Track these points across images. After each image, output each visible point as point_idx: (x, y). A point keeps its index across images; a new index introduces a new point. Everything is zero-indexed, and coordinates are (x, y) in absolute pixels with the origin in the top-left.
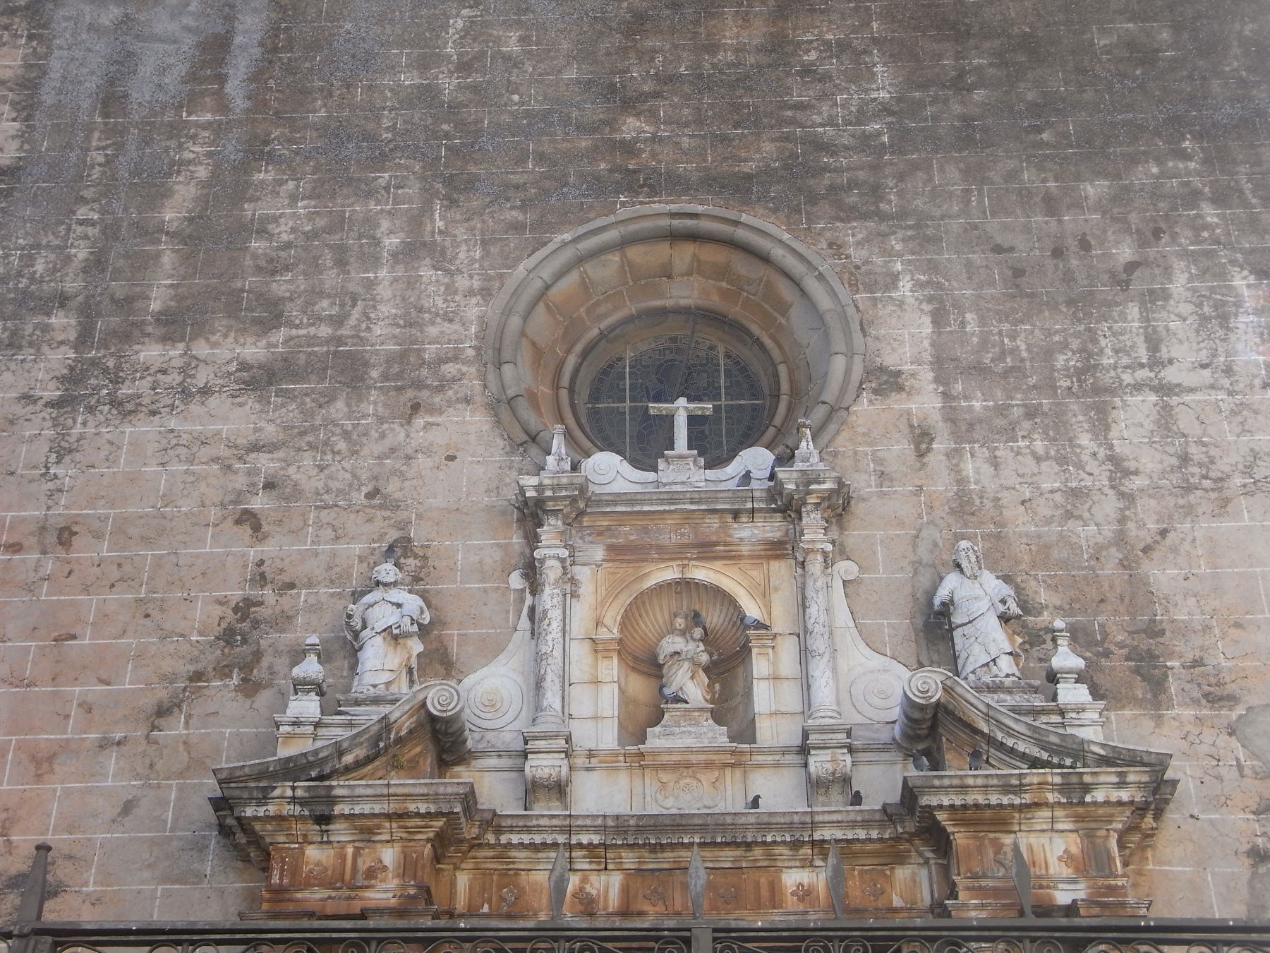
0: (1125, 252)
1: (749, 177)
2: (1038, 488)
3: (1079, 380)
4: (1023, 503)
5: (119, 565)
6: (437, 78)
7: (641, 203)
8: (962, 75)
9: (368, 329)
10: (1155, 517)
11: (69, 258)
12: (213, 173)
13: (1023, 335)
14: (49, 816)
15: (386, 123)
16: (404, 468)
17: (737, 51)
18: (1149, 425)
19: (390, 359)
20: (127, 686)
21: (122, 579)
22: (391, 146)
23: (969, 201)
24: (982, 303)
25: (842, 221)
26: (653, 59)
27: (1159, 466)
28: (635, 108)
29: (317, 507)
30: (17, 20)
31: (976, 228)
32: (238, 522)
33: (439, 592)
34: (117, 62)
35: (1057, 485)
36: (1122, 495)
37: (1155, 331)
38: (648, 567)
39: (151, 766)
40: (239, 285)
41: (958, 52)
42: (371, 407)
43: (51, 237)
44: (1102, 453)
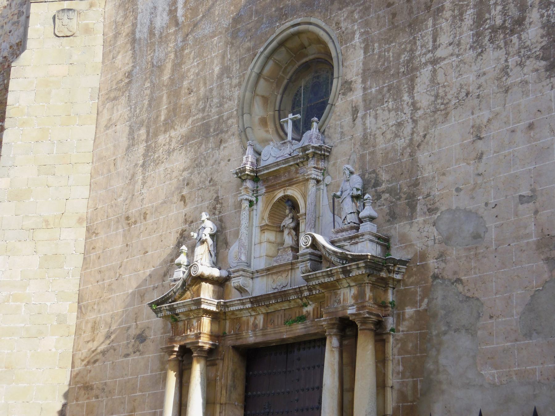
38: (276, 192)
44: (410, 101)
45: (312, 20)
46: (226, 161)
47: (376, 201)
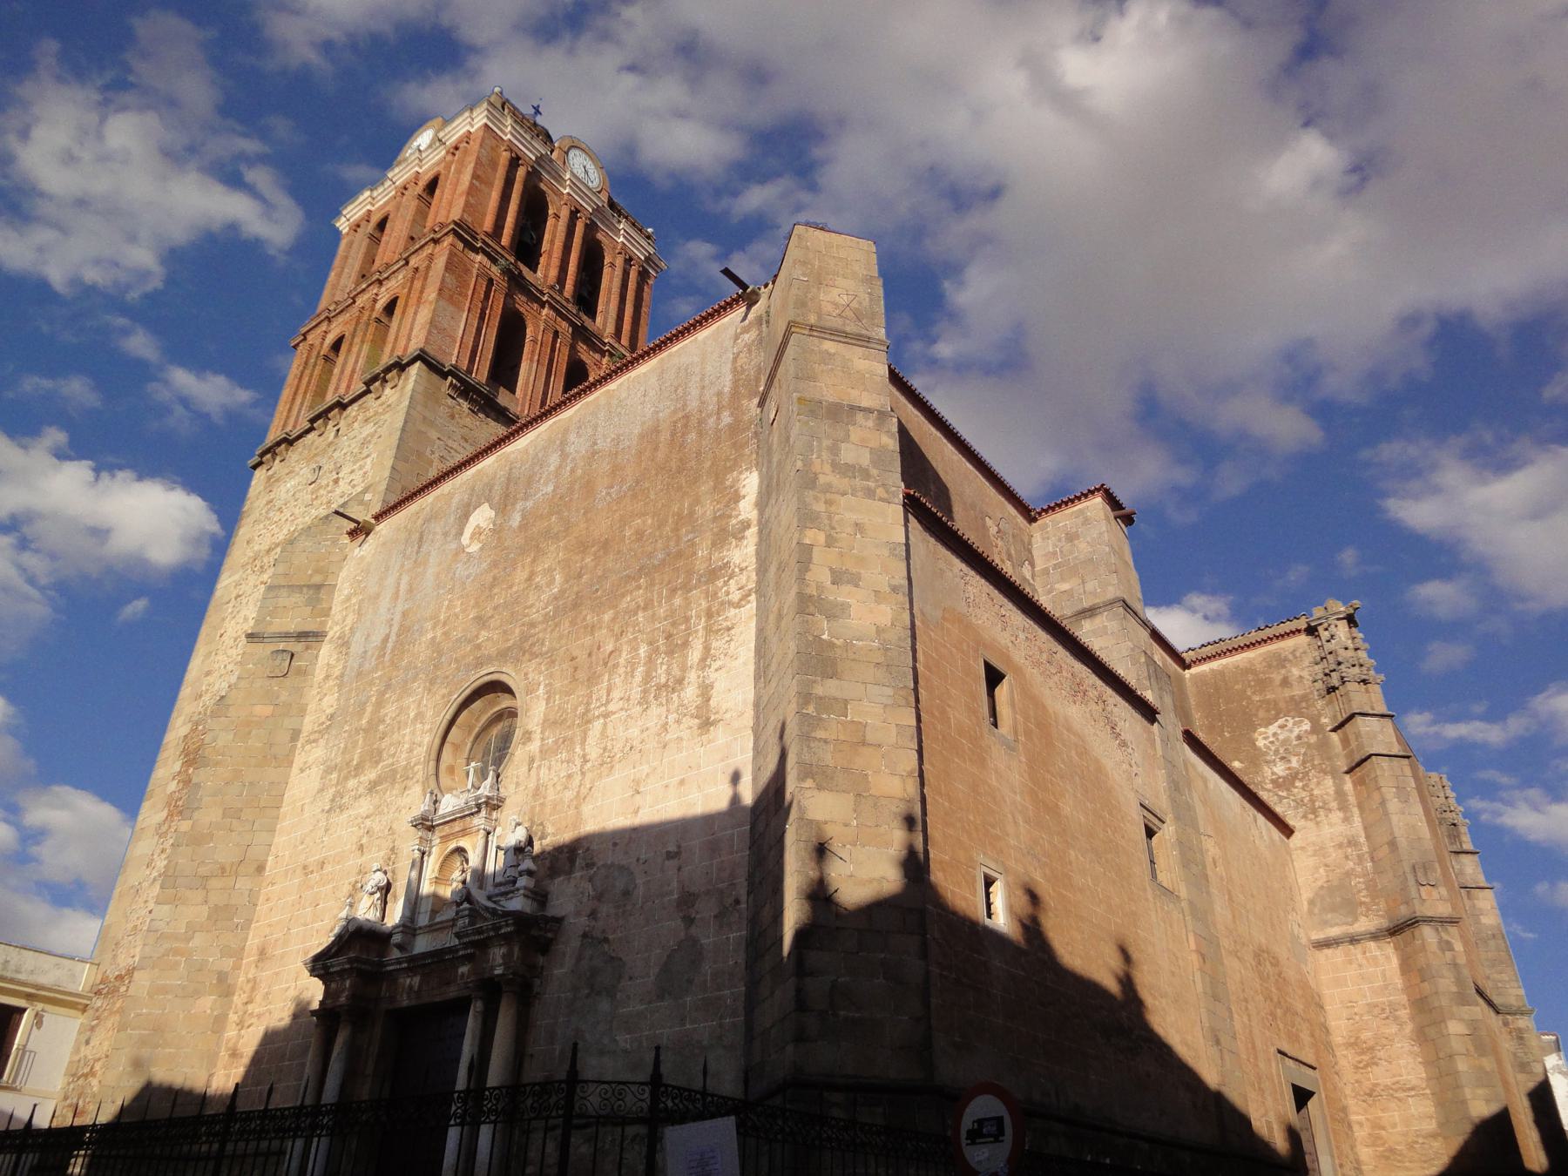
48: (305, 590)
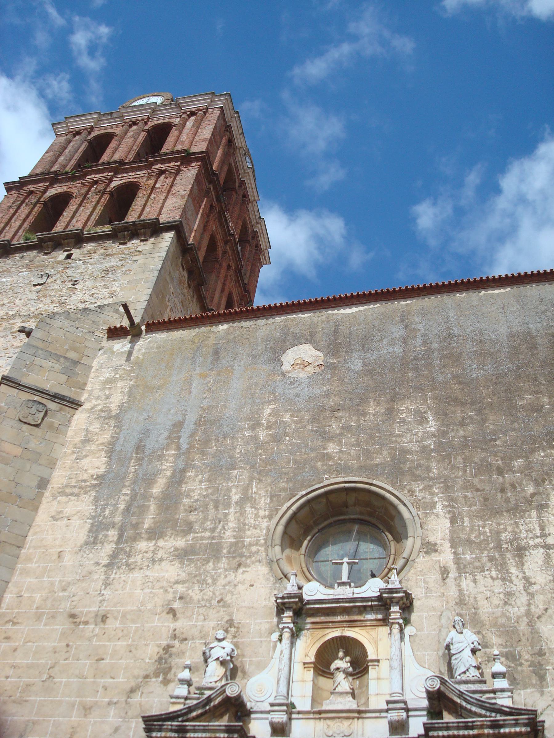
0: (531, 489)
1: (377, 465)
2: (493, 592)
3: (511, 545)
4: (487, 599)
5: (122, 631)
6: (258, 433)
7: (334, 478)
8: (464, 419)
9: (224, 533)
10: (542, 603)
11: (118, 508)
12: (172, 473)
13: (488, 526)
14: (88, 731)
15: (238, 451)
16: (233, 590)
17: (374, 415)
18: (540, 562)
19: (232, 545)
20: (120, 680)
21: (122, 636)
22: (239, 460)
23: (466, 471)
24: (471, 513)
25: (414, 481)
26: (341, 420)
27: (545, 581)
28: (333, 440)
29: (198, 607)
30: (111, 420)
31: (469, 481)
32: (168, 613)
33: (243, 642)
34: (143, 434)
35: (501, 590)
36: (529, 594)
37: (543, 522)
39: (126, 713)
40: (177, 517)
41: (463, 411)
42: (222, 565)
43: (112, 501)
44: (521, 575)
45: (374, 482)
46: (247, 585)
47: (487, 662)
48: (62, 360)
